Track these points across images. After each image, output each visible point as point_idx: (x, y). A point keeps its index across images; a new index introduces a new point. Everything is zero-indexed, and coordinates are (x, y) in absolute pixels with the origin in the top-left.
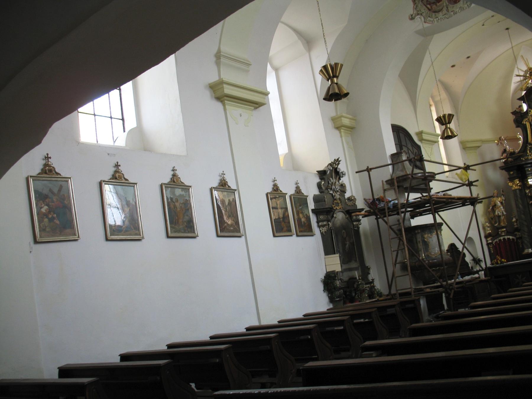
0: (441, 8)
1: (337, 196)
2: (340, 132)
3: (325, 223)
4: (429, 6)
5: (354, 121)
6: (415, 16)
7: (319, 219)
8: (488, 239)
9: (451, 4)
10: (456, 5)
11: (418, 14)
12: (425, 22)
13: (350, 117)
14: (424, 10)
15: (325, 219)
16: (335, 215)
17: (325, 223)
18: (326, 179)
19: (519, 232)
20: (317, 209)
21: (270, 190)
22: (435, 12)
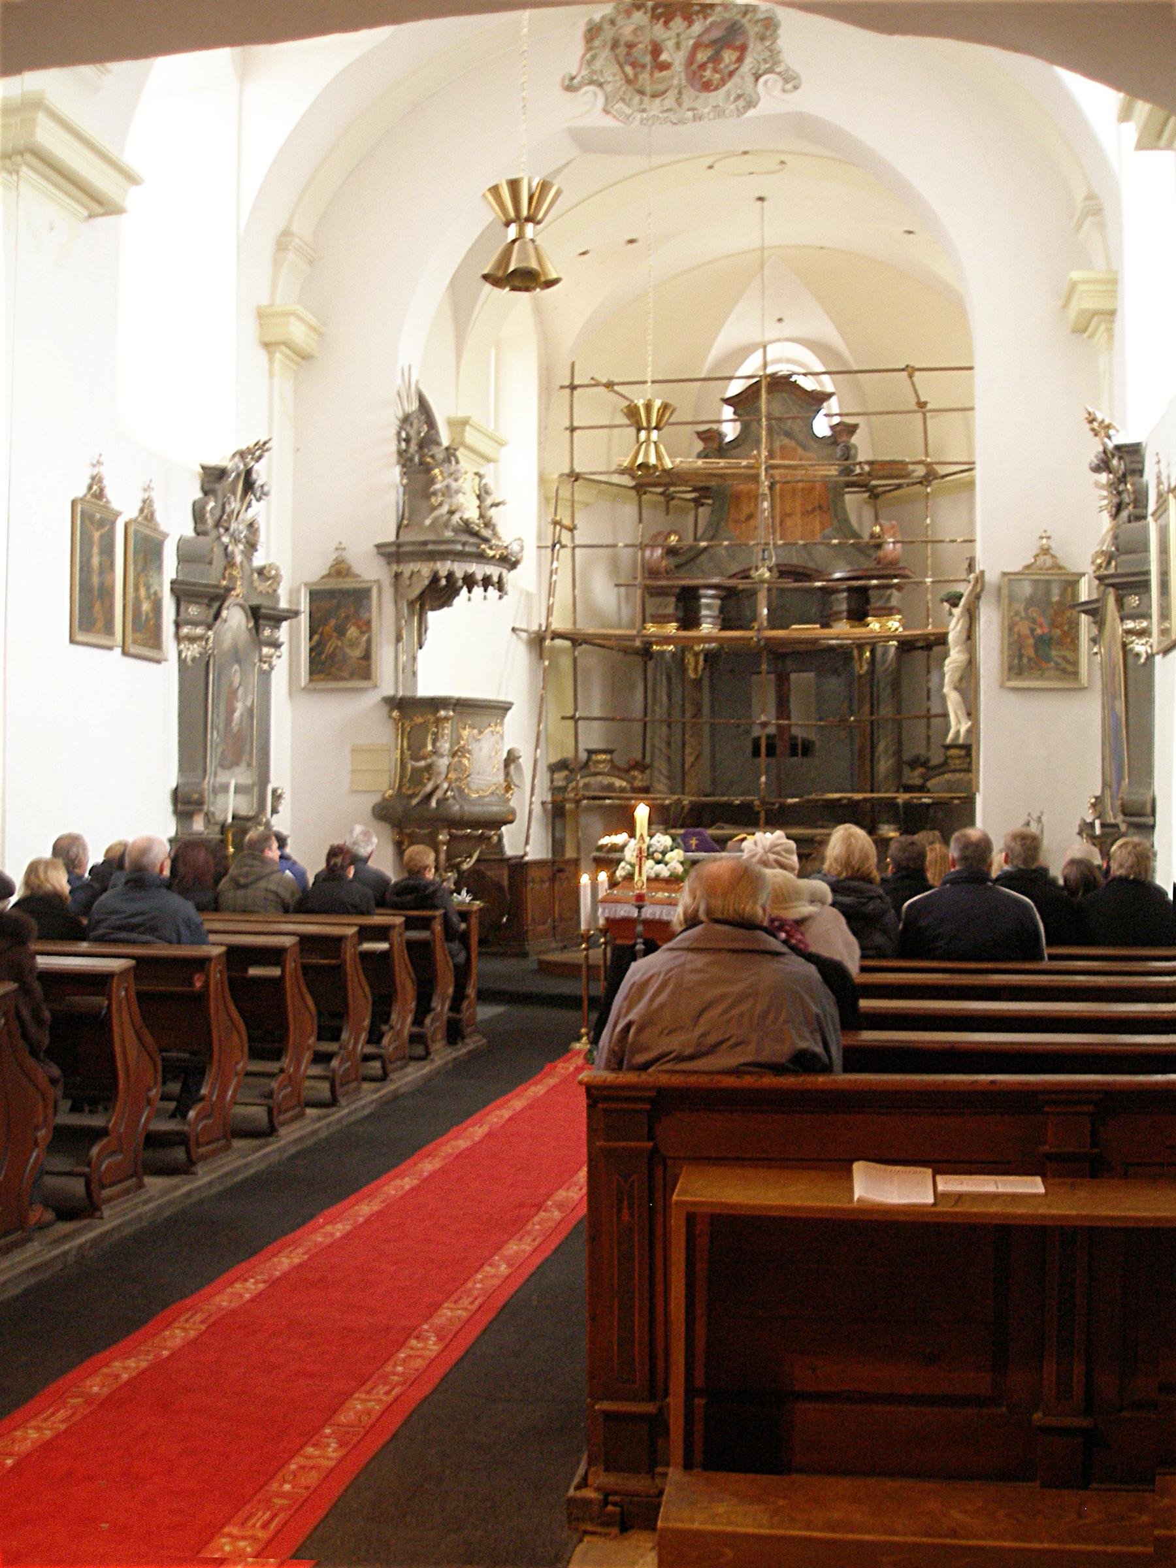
0: (662, 87)
1: (238, 551)
2: (271, 360)
3: (199, 631)
4: (629, 70)
5: (316, 338)
6: (581, 85)
7: (183, 615)
8: (556, 776)
9: (692, 86)
10: (704, 95)
11: (591, 82)
12: (606, 111)
13: (313, 321)
14: (611, 74)
15: (201, 618)
16: (224, 613)
17: (199, 631)
18: (220, 493)
19: (643, 772)
20: (183, 583)
21: (81, 491)
22: (641, 92)
